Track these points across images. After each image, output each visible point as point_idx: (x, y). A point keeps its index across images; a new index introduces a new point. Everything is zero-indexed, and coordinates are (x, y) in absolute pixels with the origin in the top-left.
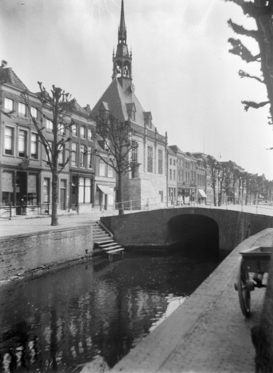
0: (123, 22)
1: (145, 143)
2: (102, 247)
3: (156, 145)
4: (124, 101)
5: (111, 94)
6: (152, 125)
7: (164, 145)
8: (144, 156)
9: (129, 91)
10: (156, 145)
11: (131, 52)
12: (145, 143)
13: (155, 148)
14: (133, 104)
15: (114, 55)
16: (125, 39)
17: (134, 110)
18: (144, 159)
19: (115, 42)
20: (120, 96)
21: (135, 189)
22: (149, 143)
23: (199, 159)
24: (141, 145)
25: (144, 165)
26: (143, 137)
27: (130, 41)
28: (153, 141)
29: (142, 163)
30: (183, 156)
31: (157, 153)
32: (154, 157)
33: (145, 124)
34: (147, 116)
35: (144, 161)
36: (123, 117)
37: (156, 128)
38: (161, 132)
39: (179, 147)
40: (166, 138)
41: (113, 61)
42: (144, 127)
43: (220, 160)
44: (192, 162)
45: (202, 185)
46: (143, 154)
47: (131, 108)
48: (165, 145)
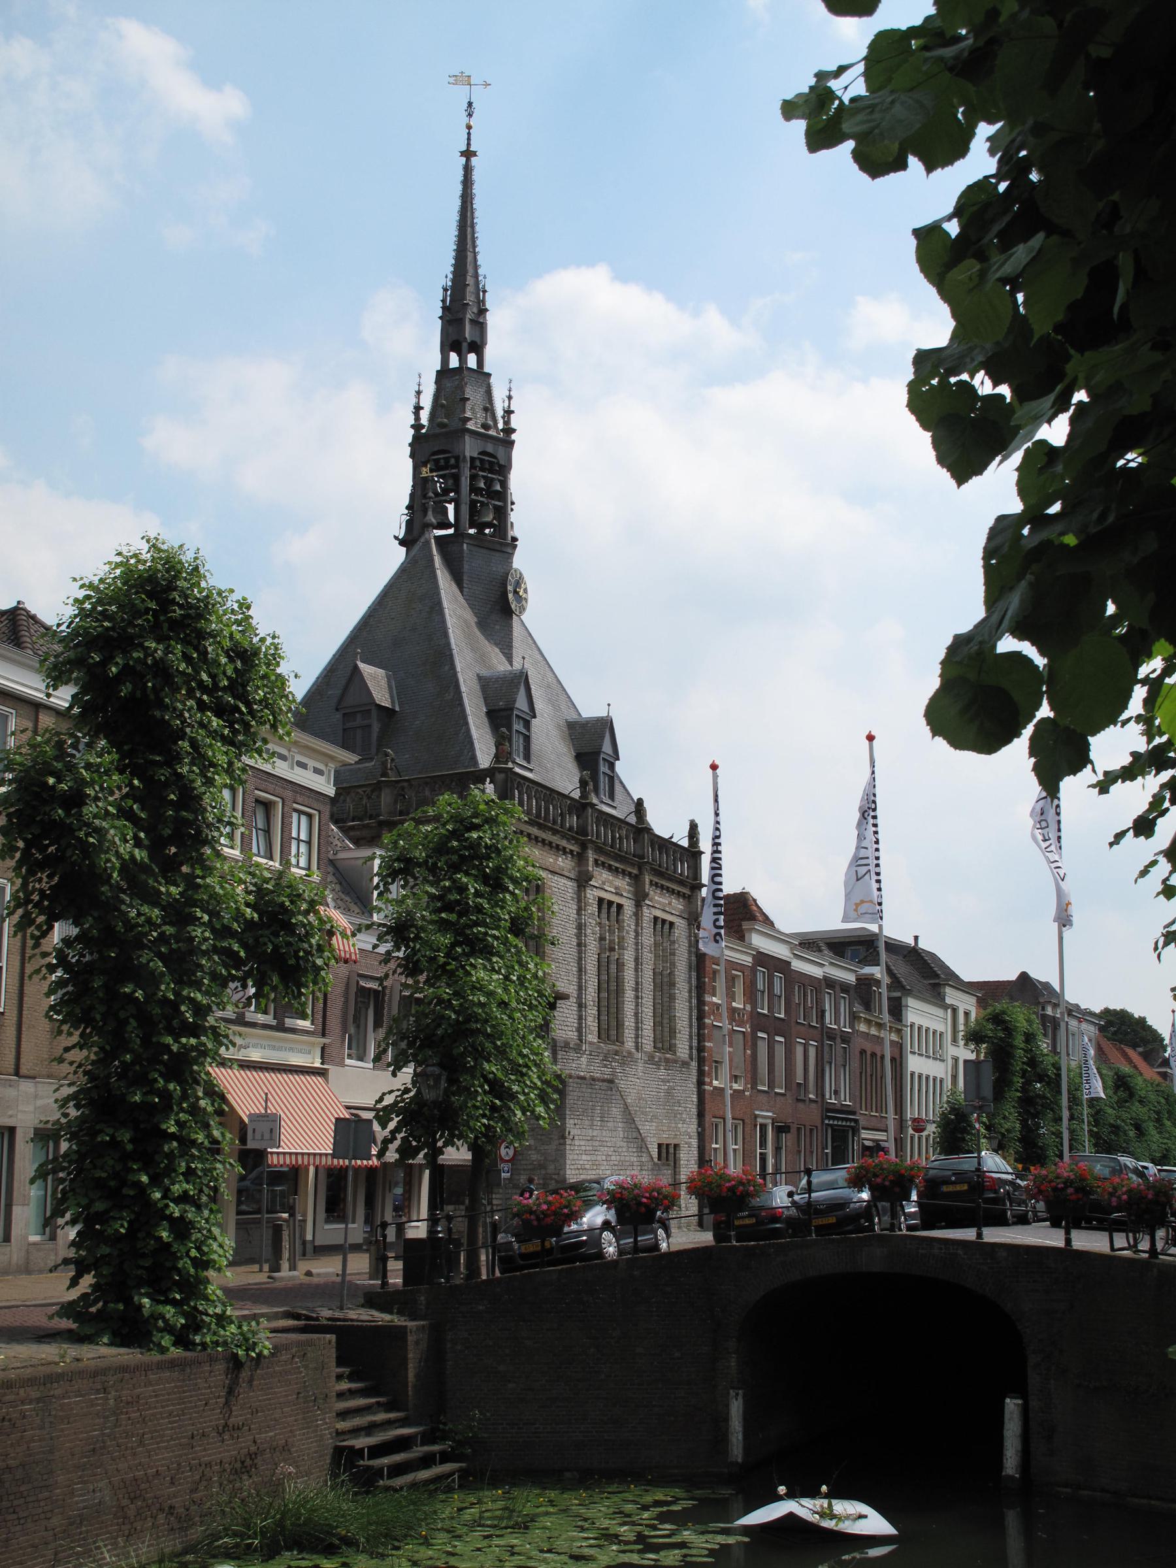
0: (470, 255)
1: (582, 881)
2: (388, 1411)
3: (640, 899)
4: (471, 659)
5: (398, 625)
6: (618, 787)
7: (684, 896)
8: (580, 952)
9: (499, 606)
10: (640, 899)
11: (508, 412)
12: (582, 881)
13: (637, 915)
14: (521, 680)
15: (418, 409)
16: (478, 347)
17: (525, 708)
18: (581, 970)
19: (421, 354)
20: (445, 604)
21: (958, 659)
22: (608, 884)
23: (867, 970)
24: (560, 890)
25: (581, 1006)
26: (571, 852)
27: (502, 350)
28: (624, 872)
29: (572, 990)
30: (780, 951)
31: (648, 938)
32: (629, 956)
33: (583, 784)
34: (593, 744)
35: (580, 978)
36: (474, 758)
37: (640, 803)
38: (667, 823)
39: (766, 901)
40: (693, 853)
41: (412, 456)
42: (576, 795)
43: (966, 980)
44: (829, 982)
45: (668, 1145)
46: (574, 942)
47: (508, 705)
48: (686, 891)
